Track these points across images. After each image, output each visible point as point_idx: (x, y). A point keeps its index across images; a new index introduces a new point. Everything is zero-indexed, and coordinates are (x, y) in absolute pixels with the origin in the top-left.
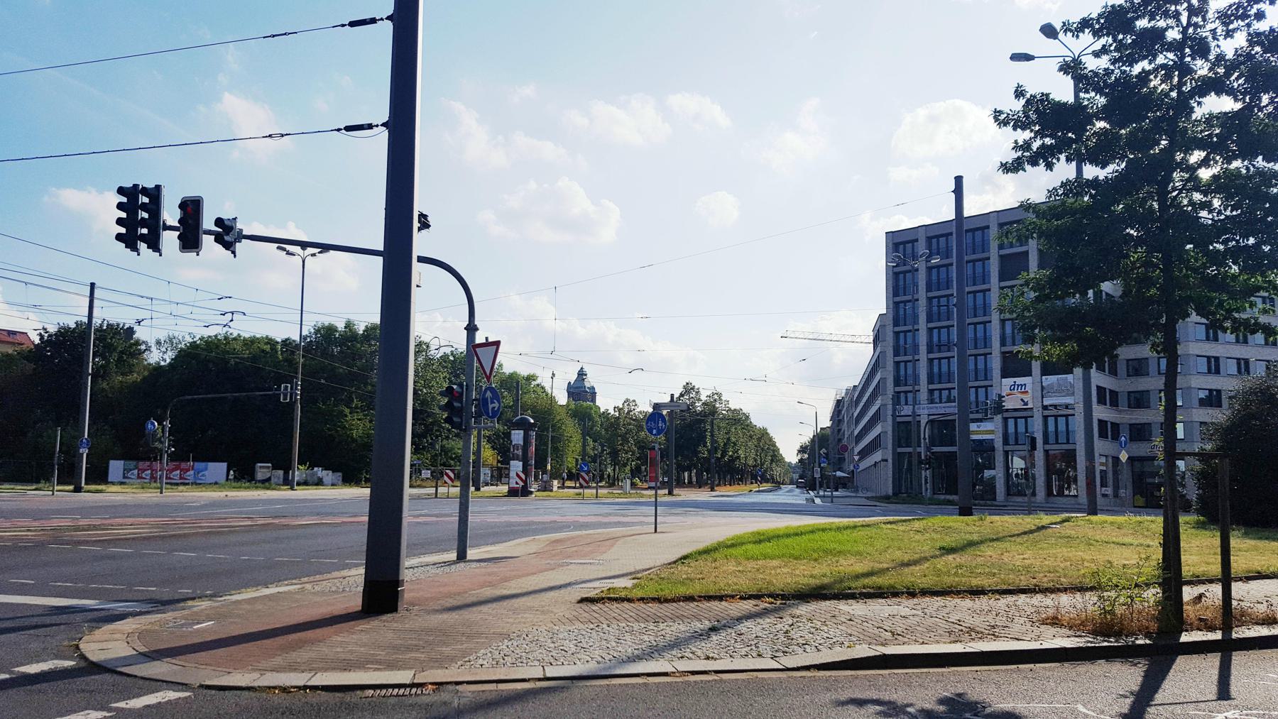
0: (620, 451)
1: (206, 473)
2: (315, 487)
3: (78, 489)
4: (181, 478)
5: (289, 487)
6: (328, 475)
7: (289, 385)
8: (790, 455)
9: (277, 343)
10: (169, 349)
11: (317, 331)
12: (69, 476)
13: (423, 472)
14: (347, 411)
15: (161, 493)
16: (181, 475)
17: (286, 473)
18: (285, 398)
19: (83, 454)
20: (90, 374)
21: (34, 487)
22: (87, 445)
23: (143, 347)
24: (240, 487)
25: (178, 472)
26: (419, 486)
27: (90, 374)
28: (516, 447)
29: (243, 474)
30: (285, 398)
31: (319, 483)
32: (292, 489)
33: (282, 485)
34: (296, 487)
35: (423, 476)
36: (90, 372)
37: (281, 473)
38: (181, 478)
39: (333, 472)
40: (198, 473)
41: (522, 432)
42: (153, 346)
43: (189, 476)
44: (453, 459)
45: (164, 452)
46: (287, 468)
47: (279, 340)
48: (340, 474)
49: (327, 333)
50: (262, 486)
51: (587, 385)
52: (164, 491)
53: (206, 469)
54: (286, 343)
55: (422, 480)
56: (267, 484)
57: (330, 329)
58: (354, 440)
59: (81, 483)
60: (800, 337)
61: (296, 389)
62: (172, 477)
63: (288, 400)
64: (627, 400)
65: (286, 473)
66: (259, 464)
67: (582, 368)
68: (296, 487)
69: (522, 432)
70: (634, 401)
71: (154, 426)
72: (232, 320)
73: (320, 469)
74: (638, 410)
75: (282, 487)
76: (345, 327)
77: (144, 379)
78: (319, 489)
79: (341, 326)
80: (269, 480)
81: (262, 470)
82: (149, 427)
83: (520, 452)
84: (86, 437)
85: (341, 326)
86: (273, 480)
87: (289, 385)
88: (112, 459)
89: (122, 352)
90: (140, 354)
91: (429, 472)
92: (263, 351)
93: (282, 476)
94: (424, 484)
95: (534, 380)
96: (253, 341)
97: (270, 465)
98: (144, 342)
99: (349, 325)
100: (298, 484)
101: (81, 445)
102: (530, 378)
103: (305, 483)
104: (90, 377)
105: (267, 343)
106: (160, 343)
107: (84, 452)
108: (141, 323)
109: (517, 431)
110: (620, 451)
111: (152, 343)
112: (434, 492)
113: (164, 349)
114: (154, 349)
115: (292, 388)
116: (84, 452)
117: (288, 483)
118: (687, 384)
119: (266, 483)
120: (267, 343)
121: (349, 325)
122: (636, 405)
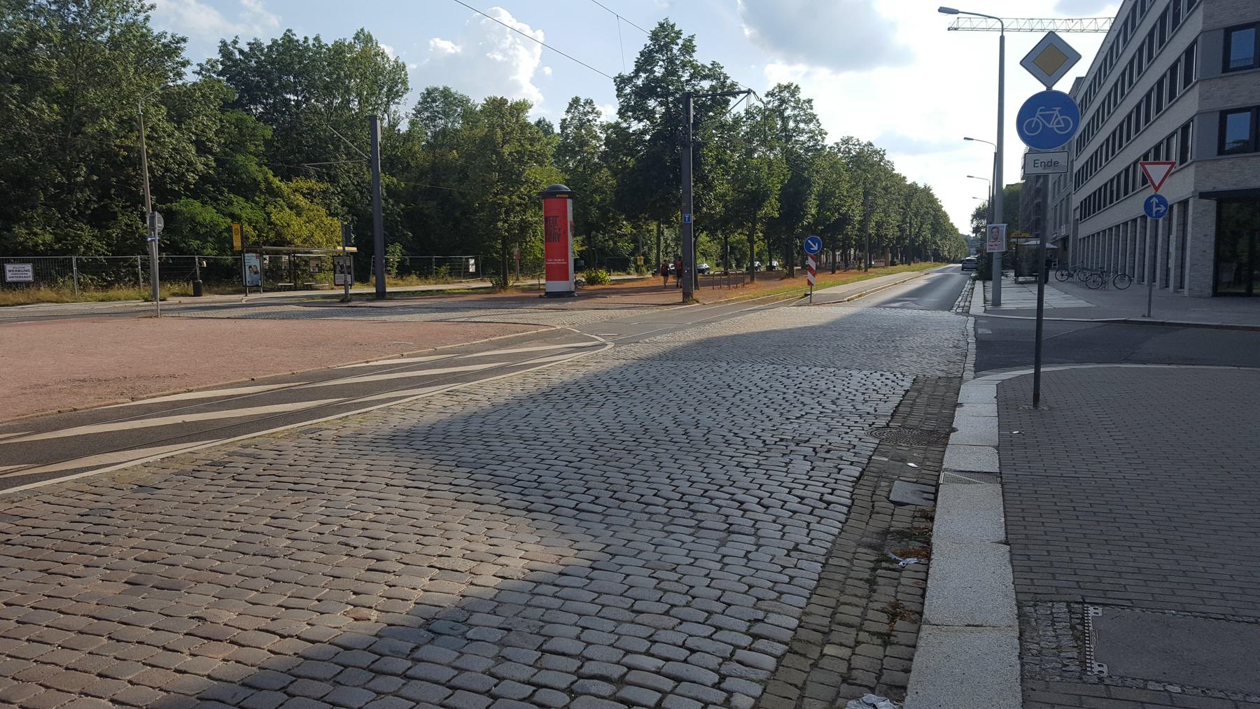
8: (963, 224)
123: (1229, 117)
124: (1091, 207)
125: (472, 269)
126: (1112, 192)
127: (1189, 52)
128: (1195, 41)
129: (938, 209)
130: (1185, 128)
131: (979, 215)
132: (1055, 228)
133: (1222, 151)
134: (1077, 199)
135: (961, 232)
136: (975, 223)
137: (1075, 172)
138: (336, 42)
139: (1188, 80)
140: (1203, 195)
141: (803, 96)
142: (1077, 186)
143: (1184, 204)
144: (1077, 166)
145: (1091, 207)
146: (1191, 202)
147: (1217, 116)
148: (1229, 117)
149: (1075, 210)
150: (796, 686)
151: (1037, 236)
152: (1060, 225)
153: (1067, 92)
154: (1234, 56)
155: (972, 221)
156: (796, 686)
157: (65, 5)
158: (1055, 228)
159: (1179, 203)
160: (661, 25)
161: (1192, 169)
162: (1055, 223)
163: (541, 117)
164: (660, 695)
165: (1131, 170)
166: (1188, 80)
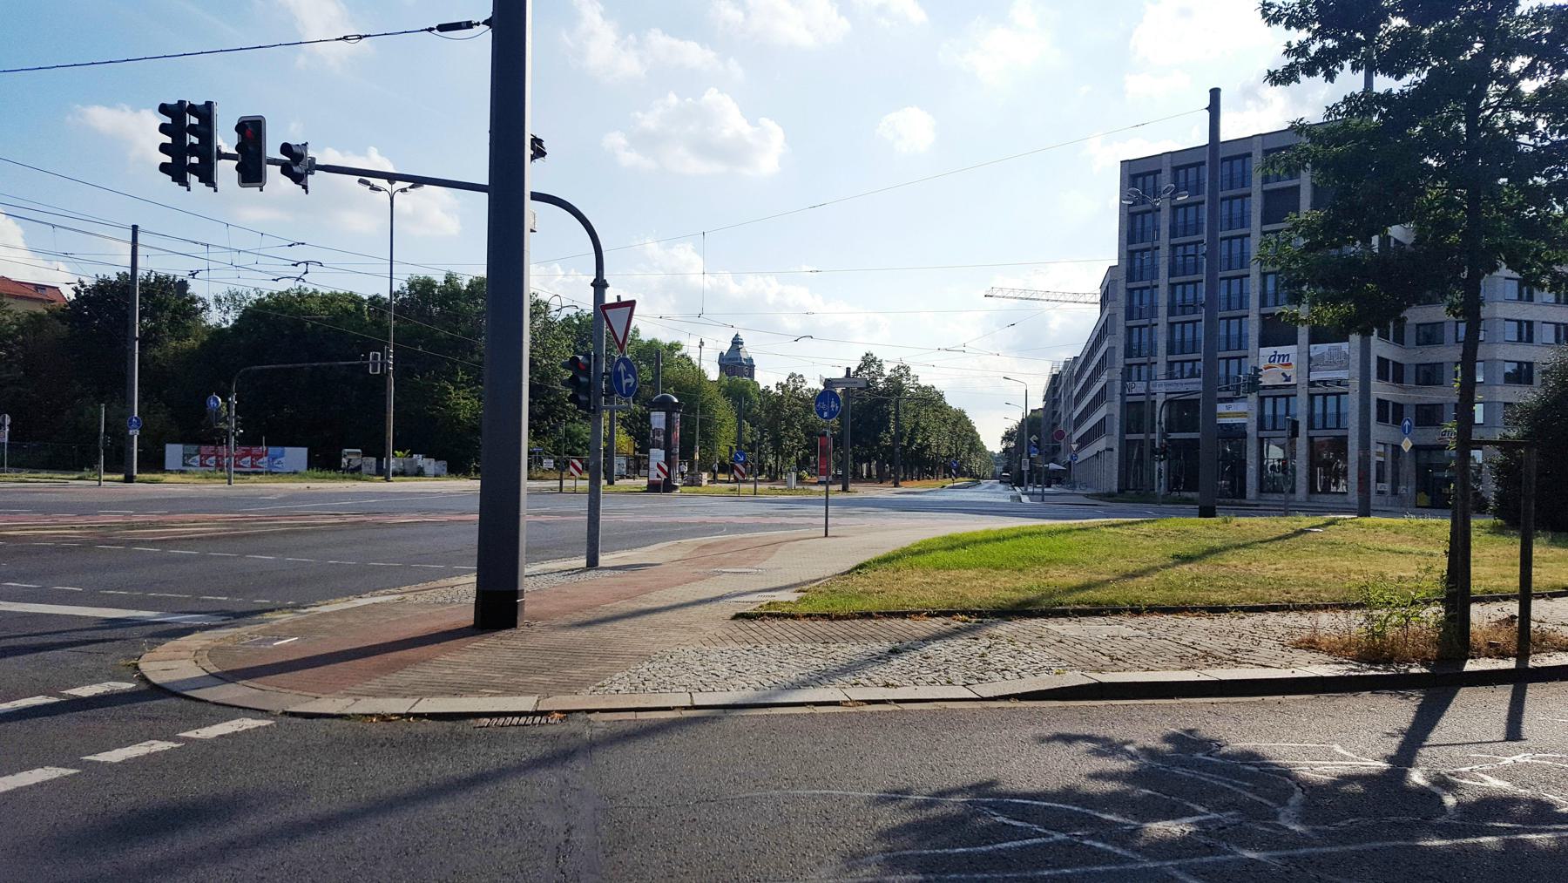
0: (782, 437)
1: (282, 459)
2: (415, 478)
3: (129, 479)
4: (253, 466)
5: (383, 478)
6: (430, 463)
7: (379, 354)
8: (993, 442)
9: (364, 301)
10: (231, 308)
11: (412, 286)
12: (117, 462)
13: (545, 461)
14: (451, 388)
15: (230, 484)
16: (252, 462)
17: (380, 461)
18: (375, 369)
19: (133, 436)
20: (137, 339)
21: (76, 476)
22: (139, 425)
23: (200, 305)
24: (325, 478)
25: (249, 458)
26: (541, 479)
27: (137, 339)
28: (657, 432)
29: (325, 461)
30: (375, 369)
31: (420, 473)
32: (387, 480)
33: (375, 476)
34: (392, 478)
35: (545, 466)
36: (137, 336)
37: (373, 460)
38: (253, 466)
39: (436, 460)
40: (274, 459)
41: (663, 414)
42: (212, 305)
43: (262, 463)
44: (579, 446)
45: (230, 434)
46: (380, 455)
47: (366, 298)
48: (445, 463)
49: (423, 288)
50: (352, 475)
51: (744, 356)
52: (233, 481)
53: (282, 455)
54: (374, 300)
55: (544, 471)
56: (357, 474)
57: (428, 284)
58: (459, 422)
59: (132, 472)
60: (1009, 295)
61: (388, 358)
62: (208, 463)
63: (378, 373)
64: (792, 375)
65: (380, 461)
66: (347, 450)
67: (737, 335)
68: (392, 478)
69: (663, 414)
70: (801, 376)
71: (218, 402)
72: (306, 272)
73: (421, 456)
74: (806, 387)
75: (375, 478)
76: (446, 282)
77: (203, 344)
78: (420, 480)
79: (440, 279)
80: (359, 468)
81: (351, 456)
82: (212, 404)
83: (661, 438)
84: (136, 415)
85: (440, 279)
86: (364, 469)
87: (379, 354)
88: (169, 443)
89: (174, 311)
90: (197, 314)
91: (552, 461)
92: (346, 310)
93: (374, 465)
94: (547, 476)
95: (678, 350)
96: (333, 298)
97: (359, 451)
98: (200, 299)
99: (450, 279)
100: (395, 474)
101: (130, 425)
102: (674, 347)
103: (403, 473)
104: (137, 343)
105: (351, 301)
106: (220, 301)
107: (135, 433)
108: (196, 276)
109: (657, 413)
110: (782, 437)
111: (211, 300)
112: (559, 485)
113: (225, 308)
114: (213, 307)
115: (382, 357)
116: (135, 433)
117: (381, 472)
118: (867, 355)
119: (355, 472)
120: (351, 301)
121: (450, 279)
122: (804, 381)
125: (1319, 490)
129: (973, 430)
131: (1008, 437)
134: (1076, 436)
135: (989, 449)
136: (1004, 444)
141: (912, 373)
142: (1075, 429)
144: (1075, 415)
145: (1084, 441)
147: (1414, 367)
150: (600, 285)
151: (1322, 489)
153: (306, 450)
155: (1002, 444)
156: (600, 285)
157: (1542, 52)
160: (867, 355)
164: (606, 311)
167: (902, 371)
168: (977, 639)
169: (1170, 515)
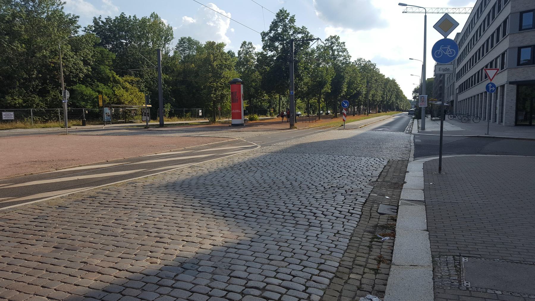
8: (409, 95)
123: (522, 50)
124: (463, 88)
126: (472, 81)
127: (505, 22)
128: (507, 18)
129: (398, 89)
130: (503, 54)
131: (416, 91)
132: (448, 97)
133: (519, 64)
134: (457, 85)
135: (408, 98)
136: (414, 94)
137: (456, 73)
138: (143, 18)
139: (504, 34)
140: (511, 83)
141: (341, 41)
142: (457, 79)
143: (503, 86)
144: (457, 70)
145: (463, 88)
146: (506, 86)
148: (522, 50)
149: (456, 89)
150: (338, 291)
151: (440, 100)
152: (450, 96)
153: (453, 39)
154: (524, 24)
155: (413, 94)
156: (338, 291)
157: (27, 2)
158: (448, 97)
159: (501, 86)
160: (281, 11)
161: (506, 72)
162: (448, 95)
163: (230, 50)
164: (280, 295)
165: (480, 72)
166: (504, 34)
167: (334, 40)
168: (25, 175)
169: (241, 128)
